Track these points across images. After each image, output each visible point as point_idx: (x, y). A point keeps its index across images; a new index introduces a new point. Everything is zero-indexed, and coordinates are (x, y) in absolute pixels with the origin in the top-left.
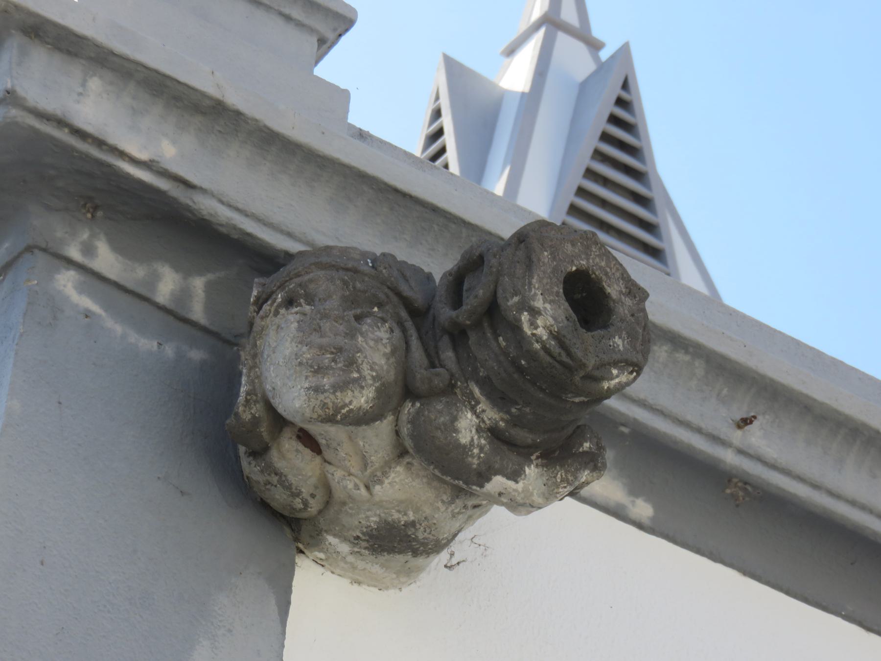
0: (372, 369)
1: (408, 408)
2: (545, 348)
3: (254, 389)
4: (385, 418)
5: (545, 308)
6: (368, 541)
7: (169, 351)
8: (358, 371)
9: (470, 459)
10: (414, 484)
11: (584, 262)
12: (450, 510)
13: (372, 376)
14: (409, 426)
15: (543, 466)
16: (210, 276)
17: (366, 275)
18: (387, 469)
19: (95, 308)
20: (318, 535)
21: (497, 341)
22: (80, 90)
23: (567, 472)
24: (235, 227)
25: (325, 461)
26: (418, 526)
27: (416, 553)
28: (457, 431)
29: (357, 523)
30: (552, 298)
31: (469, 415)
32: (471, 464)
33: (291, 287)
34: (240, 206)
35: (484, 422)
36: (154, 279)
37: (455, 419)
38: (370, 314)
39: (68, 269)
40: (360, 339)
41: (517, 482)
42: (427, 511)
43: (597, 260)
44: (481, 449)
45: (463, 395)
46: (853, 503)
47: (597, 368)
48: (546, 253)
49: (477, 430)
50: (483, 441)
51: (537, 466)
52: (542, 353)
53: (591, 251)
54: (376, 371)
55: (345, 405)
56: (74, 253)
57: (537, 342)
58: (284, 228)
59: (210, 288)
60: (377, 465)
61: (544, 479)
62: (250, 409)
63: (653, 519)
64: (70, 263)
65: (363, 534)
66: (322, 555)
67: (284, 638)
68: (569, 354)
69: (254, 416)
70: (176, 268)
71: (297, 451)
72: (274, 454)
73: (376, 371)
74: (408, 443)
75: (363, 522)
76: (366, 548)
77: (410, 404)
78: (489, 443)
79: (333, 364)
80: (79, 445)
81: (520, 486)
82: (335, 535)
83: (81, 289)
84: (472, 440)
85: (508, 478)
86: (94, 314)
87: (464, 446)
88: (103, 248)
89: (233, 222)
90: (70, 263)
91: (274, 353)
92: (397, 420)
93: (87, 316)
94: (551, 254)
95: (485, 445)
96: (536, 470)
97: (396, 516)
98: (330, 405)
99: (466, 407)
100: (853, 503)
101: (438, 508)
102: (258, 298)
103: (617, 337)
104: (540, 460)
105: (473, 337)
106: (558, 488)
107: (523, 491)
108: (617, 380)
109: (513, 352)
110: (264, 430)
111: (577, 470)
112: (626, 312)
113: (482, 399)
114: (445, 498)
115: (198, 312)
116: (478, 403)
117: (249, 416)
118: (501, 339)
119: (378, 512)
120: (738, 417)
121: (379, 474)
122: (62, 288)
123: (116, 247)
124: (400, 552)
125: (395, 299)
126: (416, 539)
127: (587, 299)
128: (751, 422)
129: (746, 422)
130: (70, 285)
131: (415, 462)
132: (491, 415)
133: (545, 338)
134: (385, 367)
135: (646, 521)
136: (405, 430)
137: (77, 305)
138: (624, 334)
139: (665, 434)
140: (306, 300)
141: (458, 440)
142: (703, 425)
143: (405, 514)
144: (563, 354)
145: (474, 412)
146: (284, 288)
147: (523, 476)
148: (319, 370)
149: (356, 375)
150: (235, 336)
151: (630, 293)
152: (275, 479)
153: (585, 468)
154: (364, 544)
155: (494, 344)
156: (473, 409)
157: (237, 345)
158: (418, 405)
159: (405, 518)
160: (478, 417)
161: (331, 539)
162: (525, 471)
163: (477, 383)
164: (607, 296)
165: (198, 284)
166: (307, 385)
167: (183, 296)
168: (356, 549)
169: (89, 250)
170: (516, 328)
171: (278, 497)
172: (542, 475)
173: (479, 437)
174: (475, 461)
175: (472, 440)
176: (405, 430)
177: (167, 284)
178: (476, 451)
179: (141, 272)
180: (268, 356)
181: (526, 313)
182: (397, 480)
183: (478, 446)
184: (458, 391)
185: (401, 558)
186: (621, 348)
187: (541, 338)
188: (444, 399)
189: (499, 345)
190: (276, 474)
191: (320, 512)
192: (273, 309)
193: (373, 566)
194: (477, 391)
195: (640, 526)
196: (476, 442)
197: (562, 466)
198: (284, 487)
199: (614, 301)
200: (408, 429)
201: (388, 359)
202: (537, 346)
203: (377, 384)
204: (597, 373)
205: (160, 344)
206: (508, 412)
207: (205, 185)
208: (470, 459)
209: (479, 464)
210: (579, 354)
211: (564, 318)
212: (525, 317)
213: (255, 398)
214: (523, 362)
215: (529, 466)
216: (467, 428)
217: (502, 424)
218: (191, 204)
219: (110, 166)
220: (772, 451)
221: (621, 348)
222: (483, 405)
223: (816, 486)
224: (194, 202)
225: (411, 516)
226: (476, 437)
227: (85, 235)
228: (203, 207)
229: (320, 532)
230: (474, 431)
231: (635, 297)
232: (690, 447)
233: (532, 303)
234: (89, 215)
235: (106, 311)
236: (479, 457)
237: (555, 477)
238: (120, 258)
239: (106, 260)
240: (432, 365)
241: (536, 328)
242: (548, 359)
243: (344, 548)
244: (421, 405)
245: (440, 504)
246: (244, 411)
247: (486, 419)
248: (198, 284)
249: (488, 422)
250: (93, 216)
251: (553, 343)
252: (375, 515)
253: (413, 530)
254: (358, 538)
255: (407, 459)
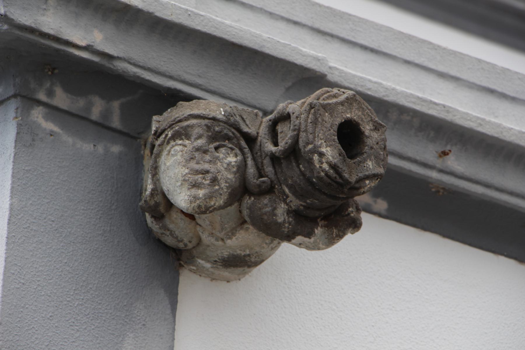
0: (226, 182)
1: (248, 201)
2: (327, 174)
3: (156, 188)
4: (234, 204)
5: (327, 151)
6: (222, 263)
7: (100, 149)
8: (219, 185)
9: (283, 229)
10: (250, 237)
11: (348, 116)
12: (270, 247)
13: (227, 186)
14: (248, 210)
15: (325, 226)
16: (123, 100)
17: (221, 121)
18: (234, 231)
19: (56, 129)
20: (192, 258)
21: (299, 167)
22: (44, 7)
23: (339, 231)
24: (138, 77)
25: (198, 224)
26: (252, 256)
27: (249, 267)
28: (275, 215)
29: (216, 255)
30: (331, 143)
31: (283, 206)
32: (284, 231)
33: (177, 128)
34: (141, 64)
35: (291, 207)
36: (88, 108)
37: (275, 209)
38: (223, 146)
39: (38, 106)
40: (219, 164)
41: (310, 238)
42: (257, 249)
43: (357, 112)
44: (290, 223)
45: (279, 193)
46: (512, 193)
47: (358, 181)
48: (327, 114)
49: (287, 213)
50: (291, 219)
51: (322, 227)
52: (325, 178)
53: (353, 106)
54: (228, 183)
55: (212, 206)
56: (42, 96)
57: (323, 171)
58: (167, 74)
59: (122, 107)
60: (229, 229)
61: (326, 235)
62: (154, 198)
63: (388, 210)
64: (39, 103)
65: (219, 259)
66: (194, 268)
67: (175, 325)
68: (341, 177)
69: (156, 202)
70: (102, 97)
71: (181, 219)
72: (167, 221)
73: (228, 183)
74: (247, 219)
75: (220, 255)
76: (220, 265)
77: (248, 197)
78: (294, 220)
79: (204, 181)
80: (53, 221)
81: (312, 240)
82: (202, 260)
83: (47, 118)
84: (285, 219)
85: (305, 237)
86: (56, 133)
87: (280, 224)
88: (59, 91)
89: (137, 74)
90: (39, 103)
91: (168, 169)
92: (240, 205)
93: (51, 135)
94: (330, 114)
95: (292, 221)
96: (321, 230)
97: (239, 252)
98: (203, 206)
99: (280, 200)
100: (512, 193)
101: (264, 247)
102: (156, 132)
103: (368, 160)
104: (323, 222)
105: (284, 164)
106: (334, 240)
107: (314, 243)
108: (369, 186)
109: (308, 174)
110: (162, 209)
111: (345, 229)
112: (374, 142)
113: (290, 195)
114: (267, 241)
115: (116, 123)
116: (287, 197)
117: (153, 203)
118: (301, 166)
119: (228, 250)
120: (440, 150)
121: (230, 234)
122: (36, 119)
123: (68, 89)
124: (240, 267)
125: (238, 135)
126: (251, 262)
127: (350, 108)
128: (448, 154)
129: (445, 154)
130: (40, 116)
131: (251, 227)
132: (295, 202)
133: (327, 169)
134: (234, 180)
135: (383, 212)
136: (245, 212)
137: (45, 129)
138: (373, 158)
139: (395, 166)
140: (186, 137)
141: (276, 220)
142: (418, 158)
143: (244, 251)
144: (338, 177)
145: (285, 202)
146: (173, 128)
147: (314, 235)
148: (195, 185)
149: (217, 187)
150: (138, 134)
151: (376, 129)
152: (168, 233)
153: (350, 227)
154: (220, 264)
155: (297, 169)
156: (285, 201)
157: (139, 138)
158: (253, 199)
159: (244, 253)
160: (287, 205)
161: (200, 261)
162: (314, 232)
163: (287, 186)
164: (362, 133)
165: (116, 105)
166: (189, 194)
167: (106, 114)
168: (215, 266)
169: (50, 93)
170: (310, 162)
171: (169, 241)
172: (325, 233)
173: (288, 218)
174: (286, 230)
175: (285, 220)
176: (245, 212)
177: (97, 108)
178: (287, 225)
179: (81, 103)
180: (165, 170)
181: (316, 155)
182: (240, 237)
183: (288, 222)
184: (276, 191)
185: (241, 269)
186: (371, 167)
187: (325, 169)
188: (268, 197)
189: (300, 170)
190: (168, 230)
191: (194, 247)
192: (166, 141)
193: (226, 273)
194: (287, 190)
195: (380, 215)
196: (287, 220)
197: (336, 227)
198: (173, 237)
199: (366, 136)
200: (247, 212)
201: (235, 174)
202: (323, 174)
203: (229, 191)
204: (357, 185)
205: (95, 145)
206: (305, 202)
207: (121, 55)
208: (283, 229)
209: (288, 232)
210: (346, 175)
211: (338, 155)
212: (316, 157)
213: (156, 192)
214: (314, 180)
215: (317, 229)
216: (281, 214)
217: (302, 208)
218: (112, 67)
219: (64, 51)
220: (462, 170)
221: (371, 167)
222: (291, 197)
223: (488, 186)
224: (114, 66)
225: (248, 252)
226: (287, 218)
227: (48, 85)
228: (119, 68)
229: (193, 257)
230: (285, 214)
231: (379, 130)
232: (410, 171)
233: (319, 149)
234: (50, 73)
235: (62, 130)
236: (288, 228)
237: (332, 234)
238: (69, 95)
239: (61, 99)
240: (261, 176)
241: (322, 163)
242: (329, 181)
243: (208, 265)
244: (255, 199)
245: (265, 245)
246: (150, 200)
247: (292, 206)
248: (116, 105)
249: (293, 207)
250: (52, 73)
251: (332, 171)
252: (227, 252)
253: (249, 258)
254: (216, 261)
255: (246, 226)
